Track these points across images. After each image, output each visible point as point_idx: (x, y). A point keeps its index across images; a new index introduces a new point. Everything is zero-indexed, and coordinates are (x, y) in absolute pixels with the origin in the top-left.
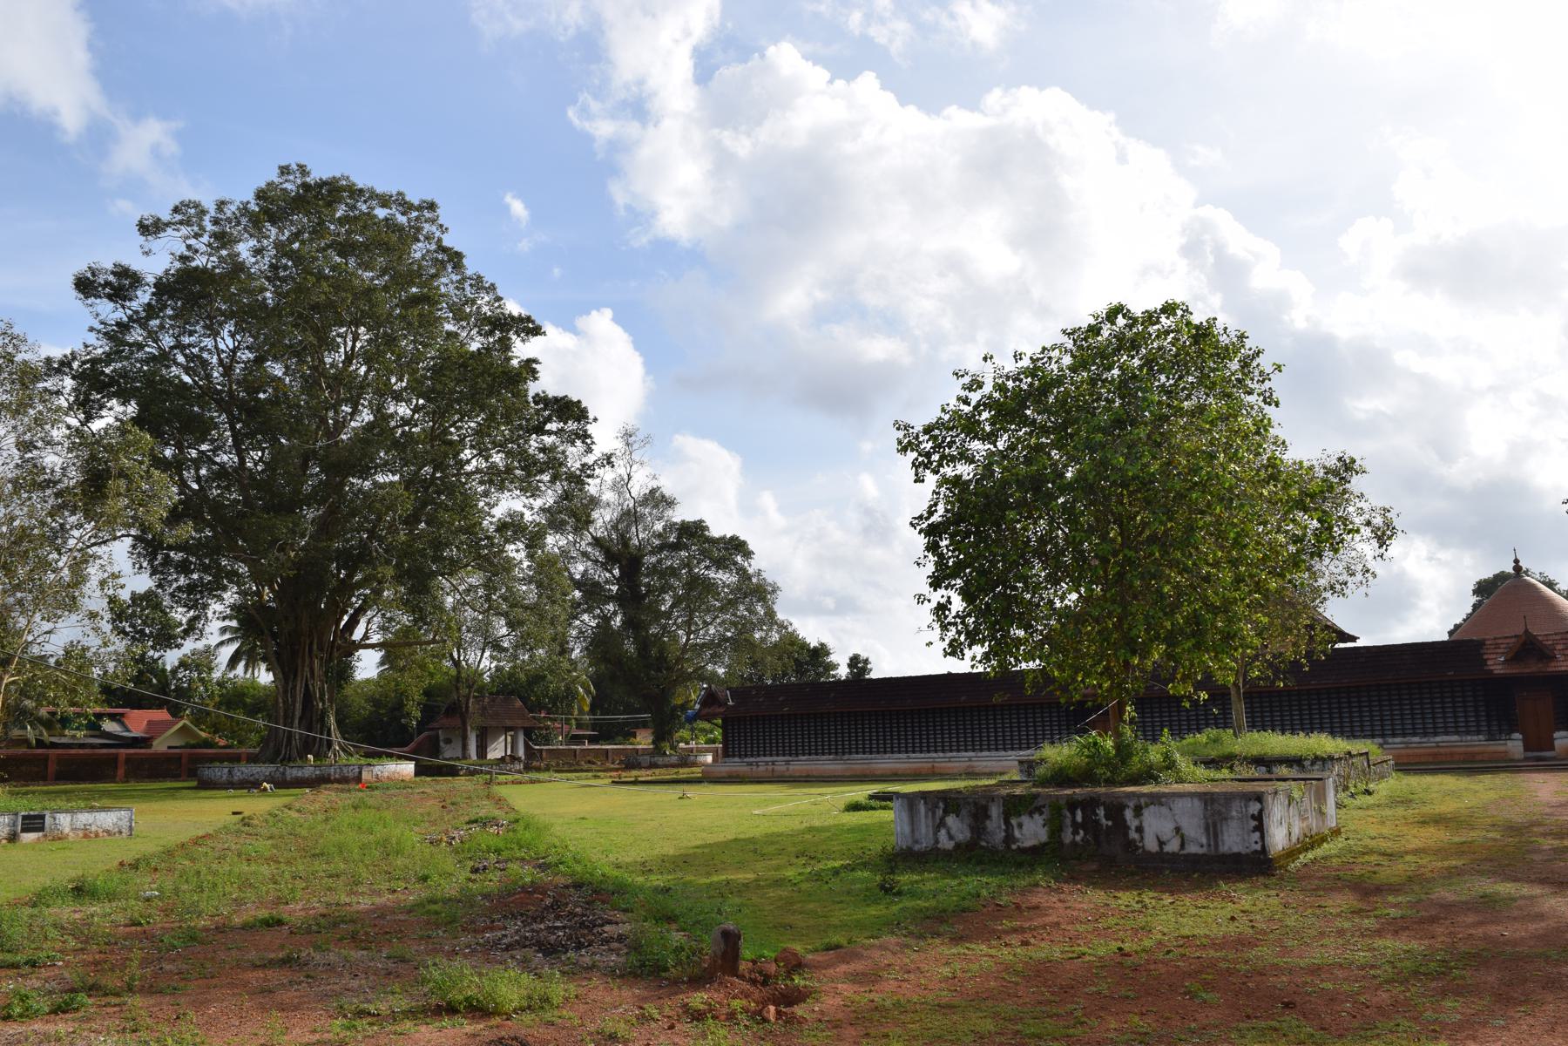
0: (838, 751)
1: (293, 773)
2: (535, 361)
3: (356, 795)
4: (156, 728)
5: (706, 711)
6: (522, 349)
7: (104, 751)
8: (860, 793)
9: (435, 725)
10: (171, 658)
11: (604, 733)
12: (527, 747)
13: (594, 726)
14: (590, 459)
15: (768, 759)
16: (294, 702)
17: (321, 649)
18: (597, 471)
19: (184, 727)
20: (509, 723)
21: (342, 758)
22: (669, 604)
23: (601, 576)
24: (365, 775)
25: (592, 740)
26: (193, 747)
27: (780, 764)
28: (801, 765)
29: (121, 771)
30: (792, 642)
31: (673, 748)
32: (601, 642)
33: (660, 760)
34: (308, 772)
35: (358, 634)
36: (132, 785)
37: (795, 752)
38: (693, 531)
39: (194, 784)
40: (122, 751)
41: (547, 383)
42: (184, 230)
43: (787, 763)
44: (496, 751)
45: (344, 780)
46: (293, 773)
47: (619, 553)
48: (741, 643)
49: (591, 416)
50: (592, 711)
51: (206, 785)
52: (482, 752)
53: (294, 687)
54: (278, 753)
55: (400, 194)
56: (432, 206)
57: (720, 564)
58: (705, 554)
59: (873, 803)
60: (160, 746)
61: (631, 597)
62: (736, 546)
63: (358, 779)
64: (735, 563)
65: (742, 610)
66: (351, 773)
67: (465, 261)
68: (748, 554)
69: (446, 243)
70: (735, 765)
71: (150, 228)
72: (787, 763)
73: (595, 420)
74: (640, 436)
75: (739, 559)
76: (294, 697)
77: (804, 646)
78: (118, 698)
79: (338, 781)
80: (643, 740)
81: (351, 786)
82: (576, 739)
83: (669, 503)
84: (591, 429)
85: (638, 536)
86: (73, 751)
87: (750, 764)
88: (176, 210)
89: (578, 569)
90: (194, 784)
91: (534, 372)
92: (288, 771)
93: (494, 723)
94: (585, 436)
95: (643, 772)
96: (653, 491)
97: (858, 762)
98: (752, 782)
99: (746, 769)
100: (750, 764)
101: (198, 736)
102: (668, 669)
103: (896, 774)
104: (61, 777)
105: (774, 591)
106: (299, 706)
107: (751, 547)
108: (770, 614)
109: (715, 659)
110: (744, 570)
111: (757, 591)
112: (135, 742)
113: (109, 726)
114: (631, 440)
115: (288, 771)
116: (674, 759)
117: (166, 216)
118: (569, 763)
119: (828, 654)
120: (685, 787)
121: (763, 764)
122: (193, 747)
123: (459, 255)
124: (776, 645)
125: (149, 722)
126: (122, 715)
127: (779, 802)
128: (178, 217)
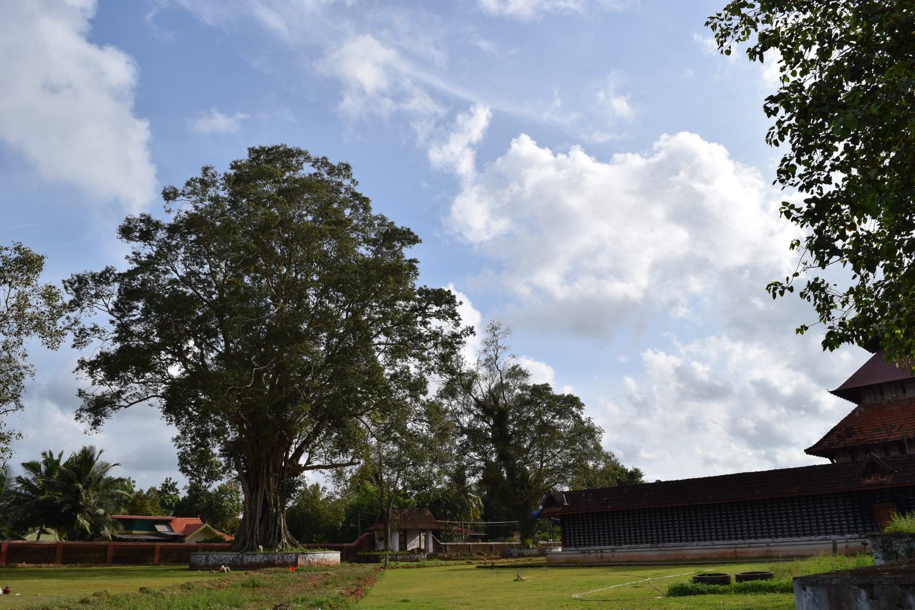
0: (654, 540)
1: (249, 559)
2: (415, 261)
3: (291, 574)
4: (189, 529)
5: (547, 510)
6: (408, 253)
7: (146, 544)
8: (685, 575)
9: (373, 528)
10: (215, 486)
11: (492, 533)
12: (436, 544)
13: (488, 529)
14: (458, 330)
15: (597, 547)
16: (256, 508)
17: (275, 470)
18: (464, 339)
19: (206, 528)
20: (421, 526)
21: (286, 546)
22: (528, 443)
23: (480, 425)
24: (300, 561)
25: (485, 539)
26: (208, 541)
27: (608, 552)
28: (624, 552)
29: (156, 557)
30: (614, 468)
31: (534, 543)
32: (490, 470)
33: (526, 552)
34: (259, 558)
35: (303, 461)
36: (162, 567)
37: (618, 541)
38: (541, 391)
39: (187, 567)
40: (158, 544)
41: (423, 280)
42: (194, 198)
43: (613, 550)
44: (413, 545)
45: (285, 565)
46: (249, 559)
47: (491, 407)
48: (580, 468)
49: (458, 301)
50: (484, 518)
51: (194, 567)
52: (403, 545)
53: (257, 497)
54: (244, 544)
55: (324, 158)
56: (347, 167)
57: (561, 413)
58: (550, 407)
59: (699, 586)
60: (190, 541)
61: (501, 437)
62: (573, 401)
63: (295, 564)
64: (572, 413)
65: (579, 446)
66: (290, 559)
67: (371, 204)
68: (580, 406)
69: (358, 190)
70: (574, 553)
71: (169, 195)
72: (613, 550)
73: (461, 303)
74: (503, 329)
75: (574, 409)
76: (256, 504)
77: (623, 471)
78: (183, 509)
79: (280, 565)
80: (516, 540)
81: (290, 570)
82: (474, 538)
83: (525, 374)
84: (458, 309)
85: (507, 398)
86: (130, 544)
87: (584, 552)
88: (188, 184)
89: (466, 420)
90: (187, 567)
91: (414, 268)
92: (245, 557)
93: (411, 527)
94: (453, 315)
95: (513, 560)
96: (514, 368)
97: (671, 549)
98: (583, 566)
99: (581, 556)
100: (584, 552)
101: (213, 533)
102: (529, 487)
103: (704, 559)
104: (116, 561)
105: (600, 433)
106: (259, 511)
107: (582, 401)
108: (598, 448)
109: (562, 479)
110: (578, 416)
111: (587, 432)
112: (175, 538)
113: (161, 528)
114: (497, 332)
115: (245, 557)
116: (535, 551)
117: (180, 187)
118: (464, 554)
119: (641, 476)
120: (520, 571)
121: (593, 552)
122: (208, 541)
123: (366, 200)
124: (603, 471)
125: (187, 526)
126: (170, 521)
127: (602, 584)
128: (190, 188)
